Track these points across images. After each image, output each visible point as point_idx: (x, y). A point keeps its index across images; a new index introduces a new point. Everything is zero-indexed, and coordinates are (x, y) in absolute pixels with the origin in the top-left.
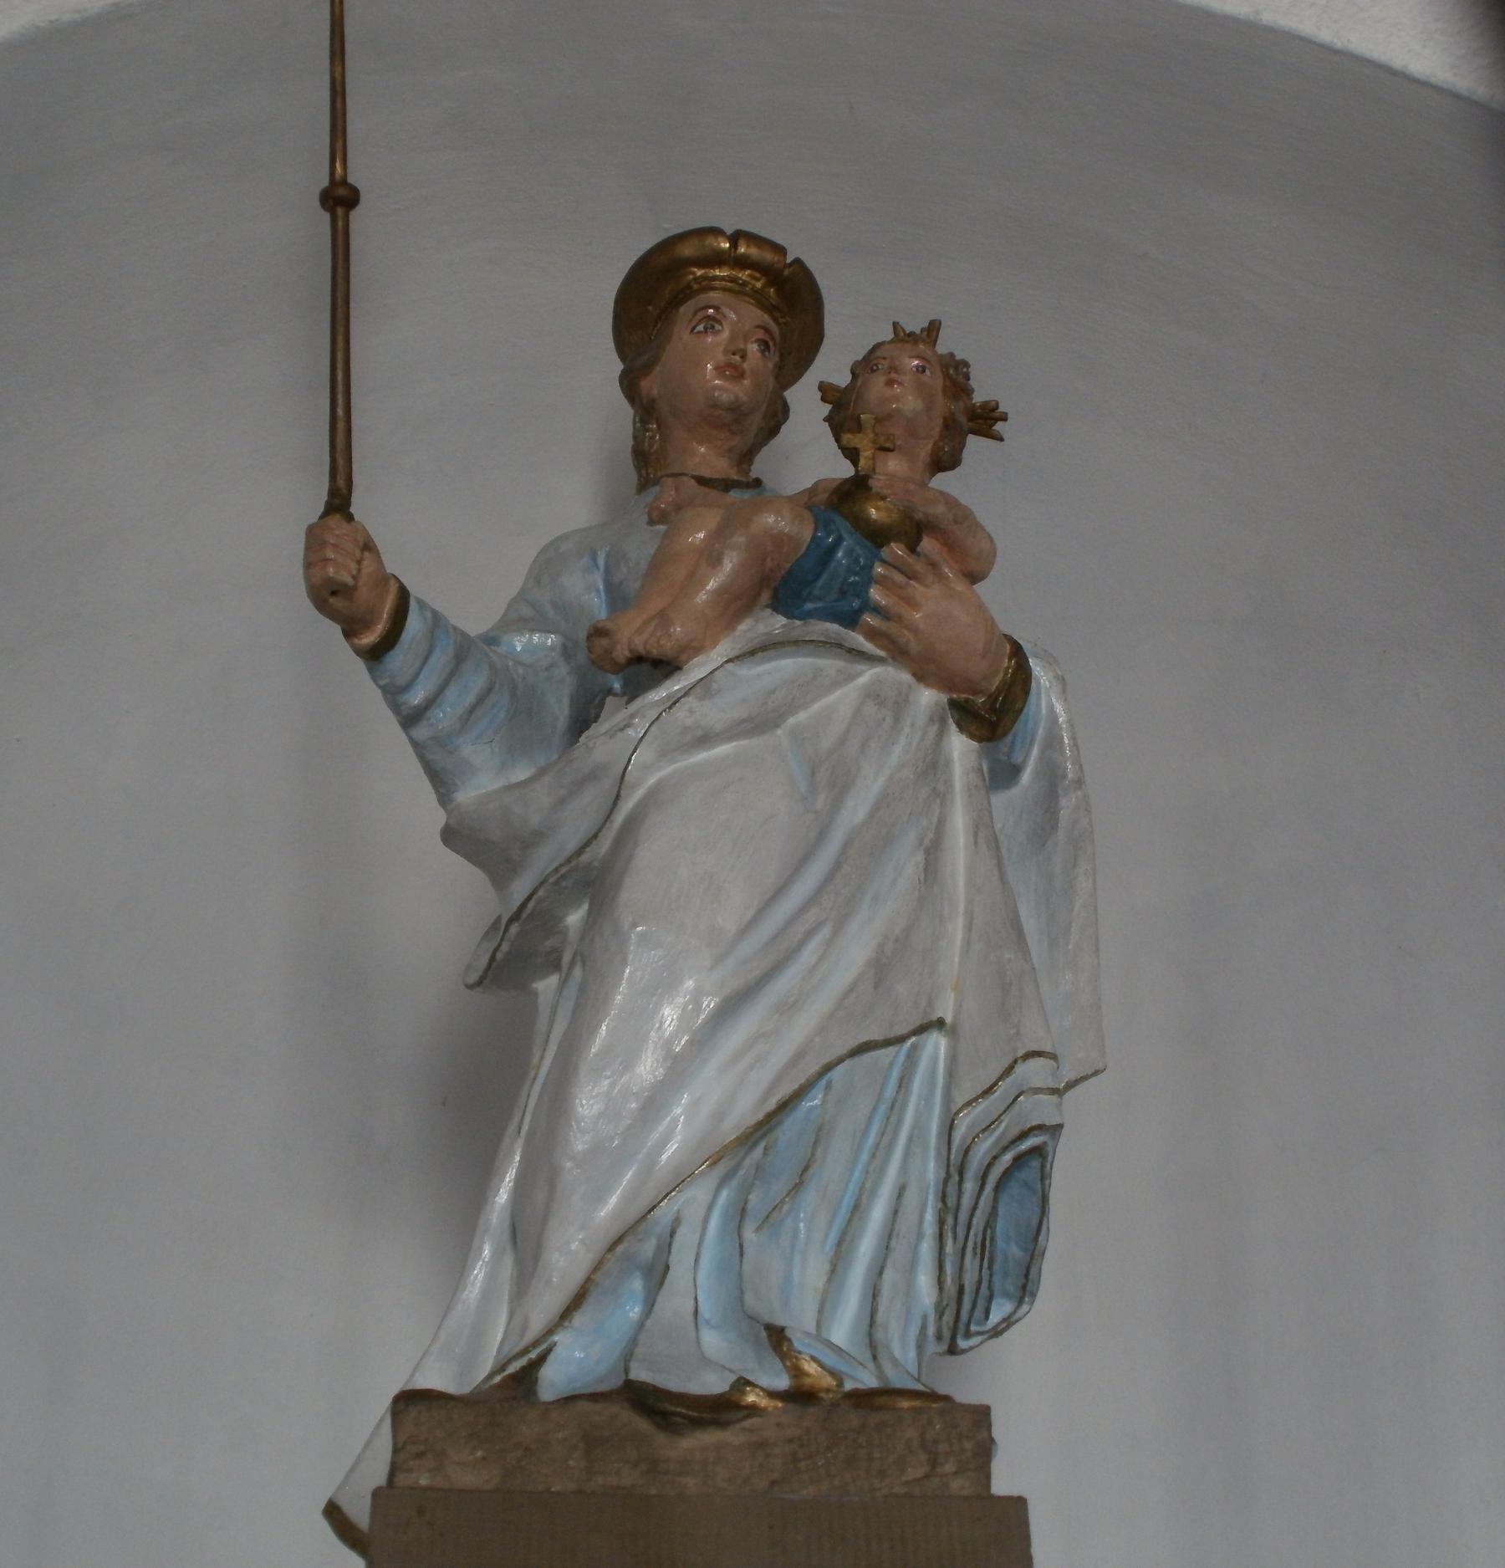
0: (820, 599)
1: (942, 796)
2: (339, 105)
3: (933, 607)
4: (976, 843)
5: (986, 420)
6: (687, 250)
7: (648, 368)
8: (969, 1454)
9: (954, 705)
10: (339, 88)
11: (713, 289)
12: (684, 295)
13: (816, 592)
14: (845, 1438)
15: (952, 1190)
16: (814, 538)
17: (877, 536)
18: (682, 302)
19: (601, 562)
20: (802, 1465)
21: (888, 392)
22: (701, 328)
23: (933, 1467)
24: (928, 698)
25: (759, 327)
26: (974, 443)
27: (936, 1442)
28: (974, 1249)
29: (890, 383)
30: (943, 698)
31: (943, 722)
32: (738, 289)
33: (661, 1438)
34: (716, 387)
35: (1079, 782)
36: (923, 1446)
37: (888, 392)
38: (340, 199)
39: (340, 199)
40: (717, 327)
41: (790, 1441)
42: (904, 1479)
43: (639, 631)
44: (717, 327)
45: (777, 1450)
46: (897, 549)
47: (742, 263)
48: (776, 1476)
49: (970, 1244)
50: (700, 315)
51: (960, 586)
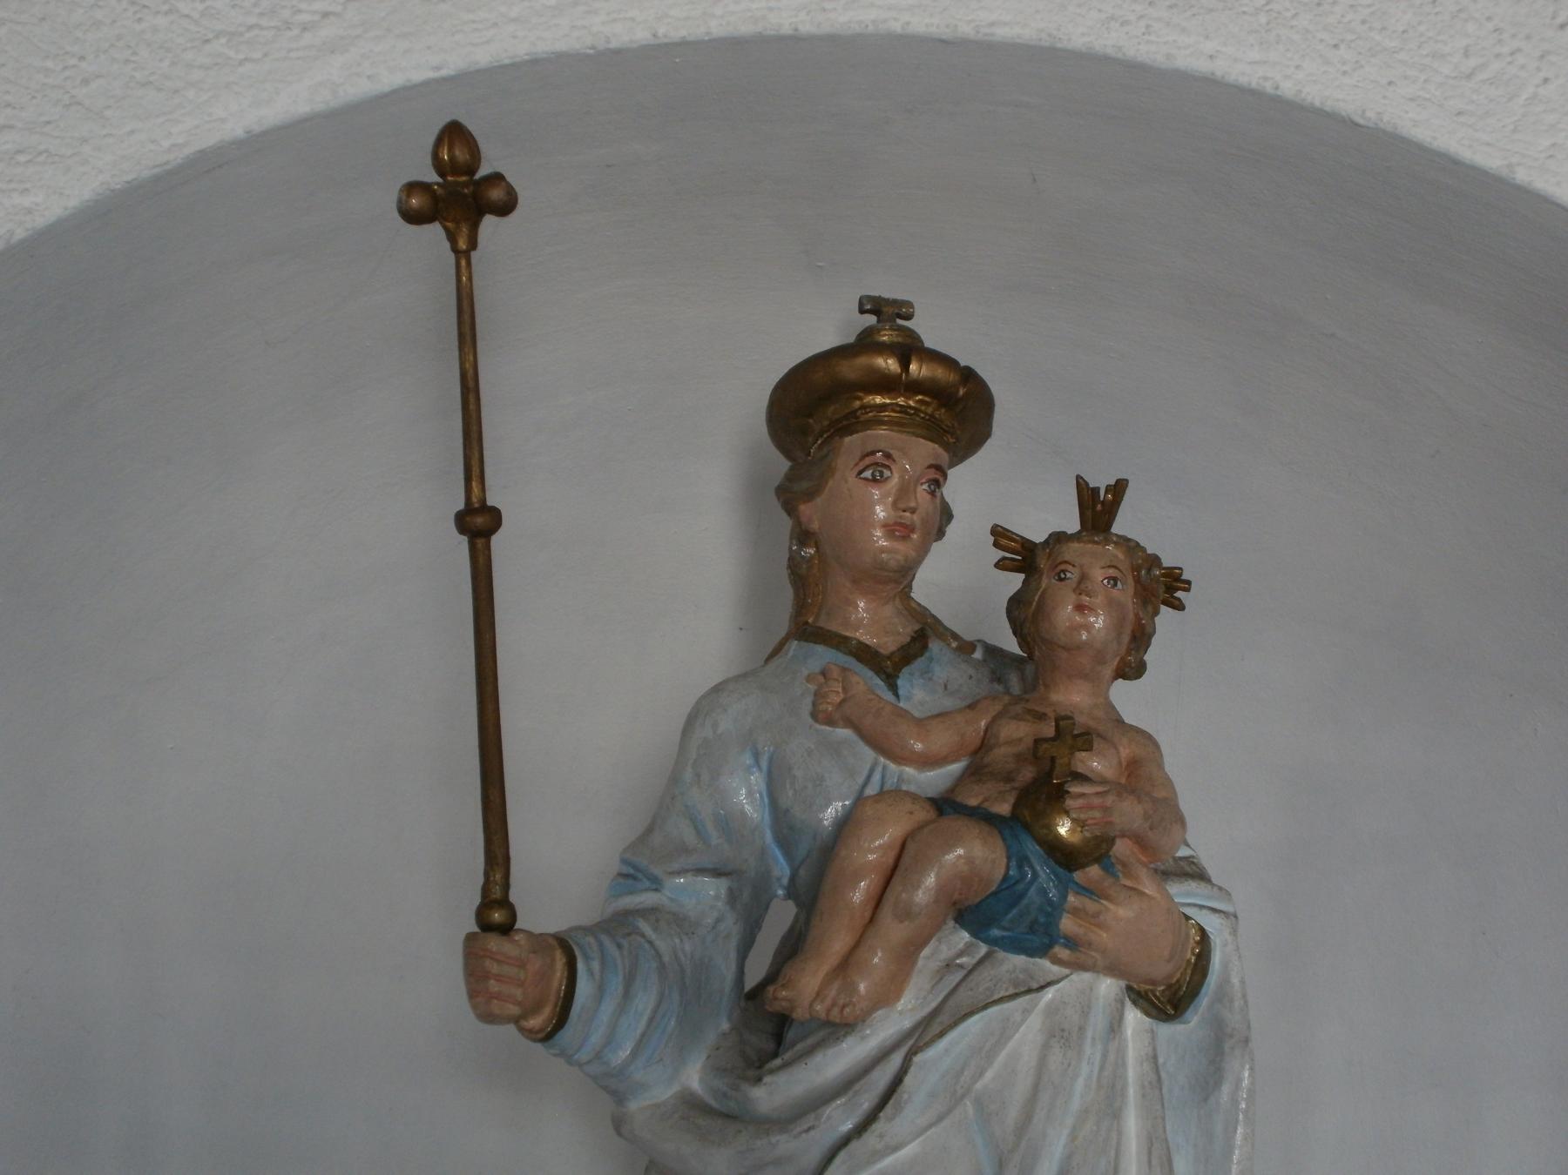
0: (1005, 929)
1: (1117, 1115)
2: (472, 407)
3: (1122, 918)
4: (1150, 1162)
6: (850, 370)
7: (810, 495)
9: (1129, 989)
10: (471, 384)
11: (879, 422)
12: (850, 424)
13: (1005, 923)
16: (1006, 878)
17: (1066, 858)
18: (849, 430)
19: (764, 764)
22: (868, 474)
24: (1108, 987)
25: (930, 467)
26: (1166, 617)
30: (1123, 983)
31: (1123, 1004)
32: (905, 421)
34: (883, 550)
38: (478, 523)
39: (478, 523)
40: (887, 473)
43: (819, 995)
44: (887, 473)
46: (1094, 871)
47: (914, 387)
50: (868, 461)
51: (1149, 888)
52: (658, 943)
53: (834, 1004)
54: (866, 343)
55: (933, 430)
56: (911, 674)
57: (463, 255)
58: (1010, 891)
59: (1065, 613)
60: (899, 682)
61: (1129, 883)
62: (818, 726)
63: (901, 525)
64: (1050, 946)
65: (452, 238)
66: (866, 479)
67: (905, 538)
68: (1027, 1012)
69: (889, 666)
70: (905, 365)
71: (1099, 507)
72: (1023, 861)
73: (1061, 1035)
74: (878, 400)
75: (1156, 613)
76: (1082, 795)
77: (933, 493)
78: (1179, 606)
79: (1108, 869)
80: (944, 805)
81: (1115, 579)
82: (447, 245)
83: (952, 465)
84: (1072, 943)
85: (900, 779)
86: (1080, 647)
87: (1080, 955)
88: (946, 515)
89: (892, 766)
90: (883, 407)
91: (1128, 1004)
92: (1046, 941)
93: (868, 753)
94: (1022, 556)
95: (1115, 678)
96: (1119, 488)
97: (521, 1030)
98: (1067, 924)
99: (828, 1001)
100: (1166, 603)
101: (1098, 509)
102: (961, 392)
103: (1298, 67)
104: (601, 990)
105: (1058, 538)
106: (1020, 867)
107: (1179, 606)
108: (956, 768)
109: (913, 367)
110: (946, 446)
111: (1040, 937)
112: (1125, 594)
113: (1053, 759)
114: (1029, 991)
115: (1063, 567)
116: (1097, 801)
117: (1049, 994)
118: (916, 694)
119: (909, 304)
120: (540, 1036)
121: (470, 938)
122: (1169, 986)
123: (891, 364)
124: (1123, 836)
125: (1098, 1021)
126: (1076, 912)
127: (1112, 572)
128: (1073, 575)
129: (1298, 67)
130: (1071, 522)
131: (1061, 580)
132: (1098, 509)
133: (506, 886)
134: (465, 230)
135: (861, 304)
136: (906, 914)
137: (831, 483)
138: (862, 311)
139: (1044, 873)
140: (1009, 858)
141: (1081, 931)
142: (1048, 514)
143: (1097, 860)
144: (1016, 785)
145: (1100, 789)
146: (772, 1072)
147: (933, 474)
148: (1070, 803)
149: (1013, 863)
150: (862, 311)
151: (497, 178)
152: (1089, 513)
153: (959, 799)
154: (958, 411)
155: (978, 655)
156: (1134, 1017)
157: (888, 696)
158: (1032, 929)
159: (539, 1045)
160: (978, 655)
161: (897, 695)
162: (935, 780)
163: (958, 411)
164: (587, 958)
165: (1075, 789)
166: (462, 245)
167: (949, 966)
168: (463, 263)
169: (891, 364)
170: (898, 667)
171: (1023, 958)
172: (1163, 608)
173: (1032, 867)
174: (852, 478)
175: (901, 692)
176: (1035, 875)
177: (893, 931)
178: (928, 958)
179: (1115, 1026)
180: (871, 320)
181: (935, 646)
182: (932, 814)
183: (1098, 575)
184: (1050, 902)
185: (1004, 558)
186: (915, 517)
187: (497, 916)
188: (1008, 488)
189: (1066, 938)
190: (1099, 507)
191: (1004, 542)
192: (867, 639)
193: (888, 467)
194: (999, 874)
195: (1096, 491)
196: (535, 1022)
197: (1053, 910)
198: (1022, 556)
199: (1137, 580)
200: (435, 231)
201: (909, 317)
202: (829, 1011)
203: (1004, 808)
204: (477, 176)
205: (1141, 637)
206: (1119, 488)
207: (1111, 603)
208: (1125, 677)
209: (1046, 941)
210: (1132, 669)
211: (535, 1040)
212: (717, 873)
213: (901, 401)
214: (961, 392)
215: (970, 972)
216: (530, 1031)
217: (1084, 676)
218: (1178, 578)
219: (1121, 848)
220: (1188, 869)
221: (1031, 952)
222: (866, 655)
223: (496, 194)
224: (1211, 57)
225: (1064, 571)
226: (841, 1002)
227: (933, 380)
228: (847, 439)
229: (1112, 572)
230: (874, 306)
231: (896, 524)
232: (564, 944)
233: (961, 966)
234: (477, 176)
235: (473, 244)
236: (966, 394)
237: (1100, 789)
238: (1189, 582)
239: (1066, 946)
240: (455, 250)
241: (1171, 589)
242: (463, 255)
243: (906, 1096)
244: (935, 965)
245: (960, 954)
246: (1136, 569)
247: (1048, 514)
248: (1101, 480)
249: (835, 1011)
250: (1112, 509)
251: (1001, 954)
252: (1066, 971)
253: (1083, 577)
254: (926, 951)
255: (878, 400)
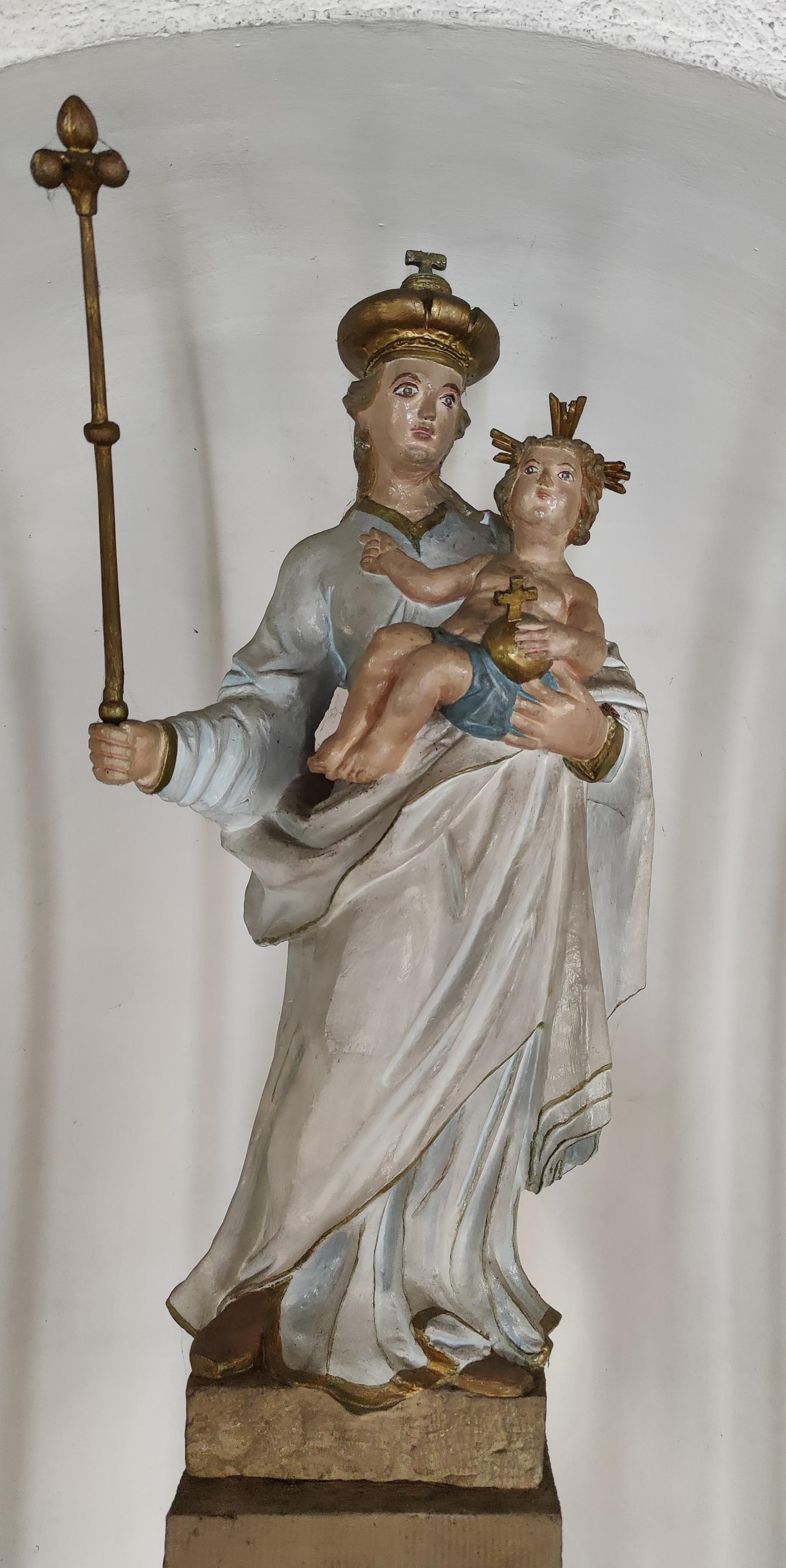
5: (614, 476)
6: (386, 310)
8: (531, 1436)
9: (564, 759)
12: (386, 354)
14: (458, 1416)
15: (539, 1140)
16: (472, 687)
17: (516, 674)
18: (388, 357)
20: (431, 1436)
21: (539, 503)
22: (401, 390)
23: (510, 1443)
27: (512, 1425)
28: (551, 1169)
29: (541, 494)
30: (561, 756)
31: (559, 770)
32: (428, 349)
33: (347, 1415)
34: (411, 448)
35: (650, 796)
36: (504, 1426)
37: (539, 503)
40: (414, 390)
41: (425, 1418)
42: (492, 1450)
44: (414, 390)
45: (417, 1423)
46: (535, 683)
47: (436, 325)
48: (414, 1442)
49: (548, 1167)
52: (247, 722)
53: (352, 771)
54: (406, 290)
55: (451, 359)
56: (431, 537)
57: (86, 218)
58: (474, 698)
59: (530, 500)
60: (421, 543)
61: (560, 690)
62: (365, 573)
63: (424, 429)
64: (504, 734)
65: (76, 201)
66: (400, 395)
67: (427, 439)
68: (489, 777)
69: (414, 531)
70: (428, 306)
71: (565, 417)
72: (484, 676)
73: (508, 792)
74: (410, 334)
75: (599, 497)
76: (528, 631)
77: (449, 405)
78: (621, 490)
79: (546, 685)
80: (439, 635)
81: (568, 473)
82: (73, 207)
83: (468, 383)
84: (519, 731)
85: (416, 612)
86: (538, 522)
87: (524, 739)
88: (464, 420)
89: (410, 601)
90: (413, 339)
91: (565, 769)
92: (501, 730)
93: (397, 591)
94: (511, 451)
95: (568, 543)
96: (580, 402)
97: (139, 786)
98: (516, 718)
99: (349, 769)
100: (607, 486)
101: (566, 417)
102: (470, 329)
103: (737, 44)
104: (197, 760)
105: (532, 440)
106: (481, 681)
107: (621, 490)
108: (456, 605)
109: (435, 309)
110: (460, 370)
111: (497, 727)
112: (575, 483)
113: (508, 605)
114: (489, 764)
115: (531, 463)
116: (537, 636)
117: (505, 764)
118: (432, 551)
119: (443, 258)
120: (151, 790)
121: (93, 727)
122: (593, 760)
123: (418, 307)
124: (557, 659)
125: (539, 783)
126: (521, 711)
127: (566, 468)
128: (538, 469)
129: (737, 44)
130: (543, 427)
131: (529, 473)
132: (566, 417)
133: (121, 692)
134: (87, 197)
135: (407, 257)
136: (404, 711)
137: (377, 396)
138: (408, 263)
139: (499, 685)
140: (474, 675)
141: (526, 724)
142: (530, 421)
143: (540, 675)
144: (488, 621)
145: (541, 627)
146: (317, 811)
147: (449, 391)
148: (519, 638)
149: (477, 677)
150: (408, 263)
151: (112, 155)
152: (558, 421)
153: (448, 630)
154: (475, 345)
155: (486, 521)
156: (568, 778)
157: (413, 554)
158: (491, 723)
159: (155, 795)
160: (486, 521)
161: (419, 553)
162: (439, 614)
163: (475, 345)
164: (186, 738)
165: (523, 627)
166: (85, 209)
167: (435, 744)
168: (87, 225)
169: (418, 307)
170: (421, 533)
171: (485, 740)
172: (606, 492)
173: (490, 681)
174: (390, 394)
175: (421, 550)
176: (492, 686)
177: (392, 722)
178: (420, 738)
179: (552, 786)
180: (415, 269)
181: (449, 516)
182: (428, 641)
183: (555, 470)
184: (502, 705)
185: (500, 454)
186: (434, 423)
187: (117, 712)
188: (509, 401)
189: (515, 727)
190: (565, 417)
191: (499, 441)
192: (406, 512)
193: (414, 385)
194: (467, 685)
195: (563, 405)
196: (147, 781)
197: (504, 710)
198: (511, 451)
199: (585, 474)
200: (62, 193)
201: (442, 268)
202: (349, 775)
203: (476, 638)
204: (96, 150)
205: (588, 515)
206: (580, 402)
207: (563, 490)
208: (576, 544)
209: (501, 730)
210: (580, 538)
211: (147, 793)
212: (291, 673)
213: (426, 335)
214: (470, 329)
215: (449, 749)
216: (145, 787)
217: (544, 544)
218: (621, 471)
219: (558, 667)
220: (617, 678)
221: (491, 737)
222: (400, 522)
223: (111, 169)
224: (664, 38)
225: (531, 467)
226: (357, 770)
227: (448, 319)
228: (388, 364)
229: (566, 468)
230: (415, 259)
231: (420, 428)
232: (169, 728)
233: (443, 745)
234: (96, 150)
235: (94, 210)
236: (473, 330)
237: (541, 627)
238: (628, 474)
239: (515, 734)
240: (81, 215)
241: (616, 478)
242: (86, 218)
243: (395, 836)
244: (428, 742)
245: (444, 737)
246: (584, 466)
247: (530, 421)
248: (567, 397)
249: (354, 775)
250: (574, 419)
251: (471, 738)
252: (518, 749)
253: (546, 473)
254: (419, 734)
255: (410, 334)
